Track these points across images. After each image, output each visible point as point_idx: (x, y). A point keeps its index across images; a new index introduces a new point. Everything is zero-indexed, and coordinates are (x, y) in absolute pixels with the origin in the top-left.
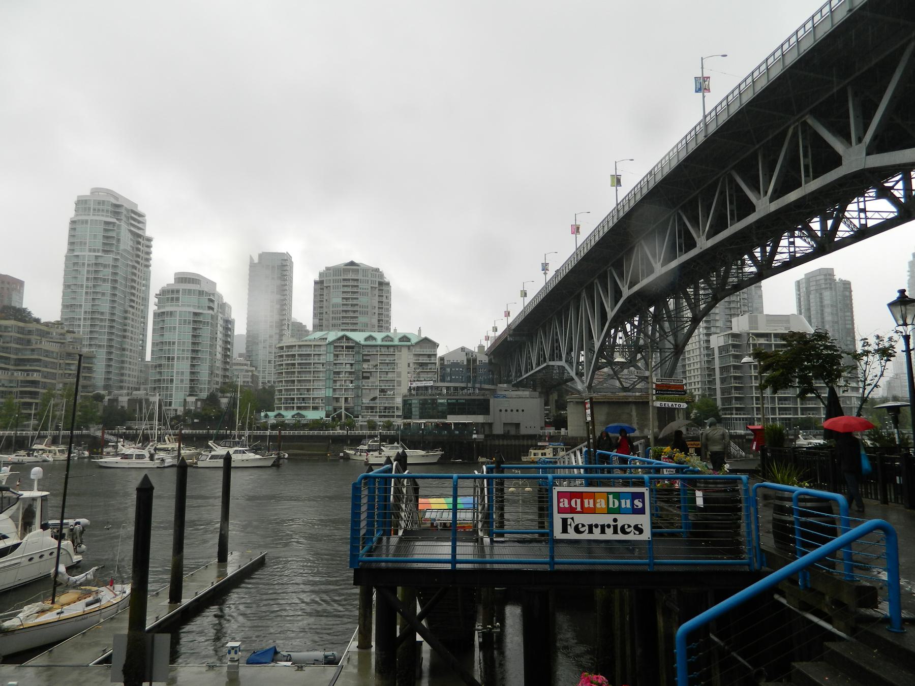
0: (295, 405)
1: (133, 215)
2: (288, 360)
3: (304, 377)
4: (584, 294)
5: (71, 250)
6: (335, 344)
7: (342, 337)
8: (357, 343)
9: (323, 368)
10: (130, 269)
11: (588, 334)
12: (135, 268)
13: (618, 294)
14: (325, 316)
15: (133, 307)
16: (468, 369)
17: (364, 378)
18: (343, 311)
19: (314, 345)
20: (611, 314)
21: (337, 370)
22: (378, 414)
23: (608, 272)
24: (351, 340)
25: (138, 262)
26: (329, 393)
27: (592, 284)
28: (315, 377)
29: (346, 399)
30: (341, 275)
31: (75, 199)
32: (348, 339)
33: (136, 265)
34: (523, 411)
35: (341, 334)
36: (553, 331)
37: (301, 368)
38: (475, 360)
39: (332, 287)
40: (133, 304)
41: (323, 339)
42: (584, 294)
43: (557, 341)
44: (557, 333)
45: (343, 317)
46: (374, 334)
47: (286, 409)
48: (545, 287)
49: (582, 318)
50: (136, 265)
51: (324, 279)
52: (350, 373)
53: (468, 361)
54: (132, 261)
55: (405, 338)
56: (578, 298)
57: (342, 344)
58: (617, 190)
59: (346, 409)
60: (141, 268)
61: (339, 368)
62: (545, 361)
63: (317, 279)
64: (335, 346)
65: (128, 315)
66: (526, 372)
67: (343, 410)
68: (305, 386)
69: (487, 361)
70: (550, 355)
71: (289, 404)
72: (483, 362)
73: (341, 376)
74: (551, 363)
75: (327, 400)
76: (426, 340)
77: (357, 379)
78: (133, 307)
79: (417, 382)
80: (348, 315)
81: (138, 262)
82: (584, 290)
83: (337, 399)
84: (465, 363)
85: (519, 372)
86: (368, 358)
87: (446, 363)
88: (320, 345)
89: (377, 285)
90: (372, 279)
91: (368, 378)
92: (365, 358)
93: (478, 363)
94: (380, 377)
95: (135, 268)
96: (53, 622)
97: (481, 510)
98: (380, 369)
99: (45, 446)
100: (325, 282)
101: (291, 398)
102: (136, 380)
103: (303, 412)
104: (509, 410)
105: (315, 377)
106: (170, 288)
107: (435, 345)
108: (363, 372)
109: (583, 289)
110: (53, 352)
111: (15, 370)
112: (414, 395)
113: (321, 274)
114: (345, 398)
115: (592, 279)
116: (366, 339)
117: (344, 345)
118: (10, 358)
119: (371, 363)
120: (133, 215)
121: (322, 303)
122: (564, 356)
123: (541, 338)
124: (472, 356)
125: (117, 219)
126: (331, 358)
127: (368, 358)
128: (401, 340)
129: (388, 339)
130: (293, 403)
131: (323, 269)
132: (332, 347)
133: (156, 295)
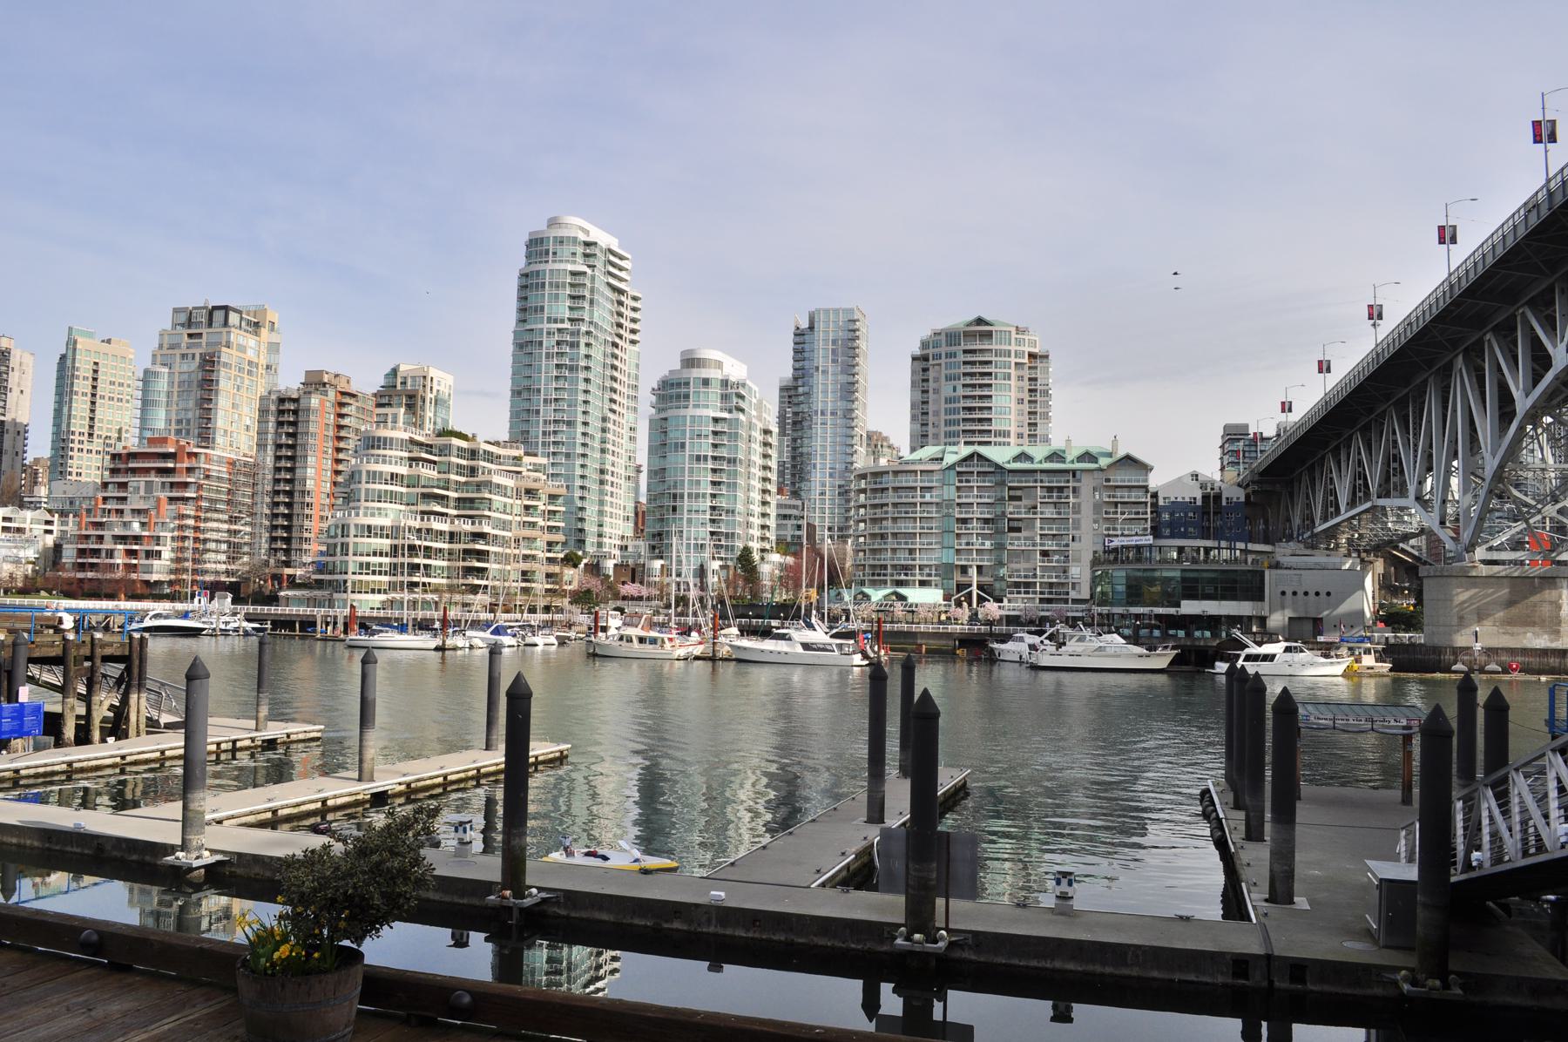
0: (888, 578)
1: (612, 258)
2: (875, 498)
3: (904, 527)
4: (1460, 362)
5: (522, 321)
6: (958, 469)
7: (971, 457)
8: (997, 466)
9: (937, 512)
10: (609, 350)
11: (1468, 443)
12: (615, 345)
13: (1541, 361)
14: (931, 418)
15: (614, 411)
16: (1204, 513)
17: (1011, 530)
18: (964, 408)
19: (921, 471)
20: (1522, 404)
21: (963, 516)
22: (1039, 596)
23: (1519, 319)
24: (987, 460)
25: (620, 337)
26: (949, 557)
27: (1480, 342)
28: (922, 528)
29: (979, 568)
30: (960, 344)
31: (526, 238)
32: (980, 457)
33: (617, 340)
34: (1328, 594)
35: (966, 451)
36: (1387, 440)
37: (898, 512)
38: (1218, 497)
39: (943, 366)
40: (614, 407)
41: (937, 459)
42: (1460, 362)
43: (1397, 458)
44: (1395, 442)
45: (964, 420)
46: (1030, 450)
47: (874, 584)
48: (1377, 354)
49: (1455, 411)
50: (617, 340)
51: (931, 351)
52: (986, 521)
53: (1205, 497)
54: (610, 334)
55: (1087, 456)
56: (1446, 372)
57: (971, 469)
58: (1546, 151)
59: (980, 587)
60: (625, 346)
61: (966, 512)
62: (1367, 496)
63: (918, 352)
64: (959, 473)
65: (610, 425)
66: (1325, 519)
67: (974, 587)
68: (906, 543)
69: (1243, 499)
70: (1380, 486)
71: (879, 575)
72: (1235, 500)
73: (968, 526)
74: (1381, 502)
75: (946, 570)
76: (1129, 461)
77: (999, 532)
78: (614, 411)
79: (1123, 538)
80: (974, 416)
81: (620, 337)
82: (1460, 358)
83: (964, 570)
84: (1199, 503)
85: (1309, 521)
86: (1018, 493)
87: (1161, 503)
88: (932, 471)
89: (1026, 360)
90: (1018, 348)
91: (1019, 530)
92: (1012, 493)
93: (1224, 503)
94: (1041, 529)
95: (615, 345)
96: (949, 853)
97: (1311, 770)
98: (1042, 513)
99: (642, 628)
100: (931, 358)
101: (881, 565)
102: (385, 543)
103: (902, 591)
104: (1300, 593)
105: (922, 528)
106: (675, 377)
107: (1145, 468)
108: (1009, 520)
109: (1457, 355)
110: (506, 487)
111: (458, 516)
112: (24, 630)
113: (924, 345)
114: (978, 567)
115: (1481, 333)
116: (1017, 458)
117: (976, 470)
118: (448, 497)
119: (1025, 502)
120: (612, 258)
121: (925, 395)
122: (1412, 489)
123: (1359, 453)
124: (1212, 489)
125: (589, 266)
126: (950, 493)
127: (1018, 493)
128: (1081, 458)
129: (1056, 456)
130: (885, 575)
131: (926, 333)
132: (953, 473)
133: (653, 389)
